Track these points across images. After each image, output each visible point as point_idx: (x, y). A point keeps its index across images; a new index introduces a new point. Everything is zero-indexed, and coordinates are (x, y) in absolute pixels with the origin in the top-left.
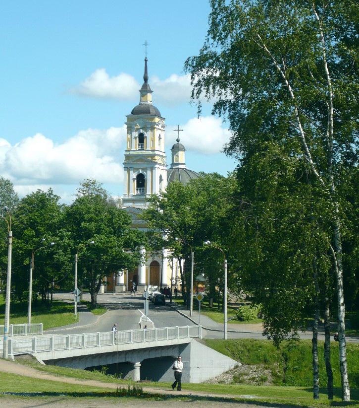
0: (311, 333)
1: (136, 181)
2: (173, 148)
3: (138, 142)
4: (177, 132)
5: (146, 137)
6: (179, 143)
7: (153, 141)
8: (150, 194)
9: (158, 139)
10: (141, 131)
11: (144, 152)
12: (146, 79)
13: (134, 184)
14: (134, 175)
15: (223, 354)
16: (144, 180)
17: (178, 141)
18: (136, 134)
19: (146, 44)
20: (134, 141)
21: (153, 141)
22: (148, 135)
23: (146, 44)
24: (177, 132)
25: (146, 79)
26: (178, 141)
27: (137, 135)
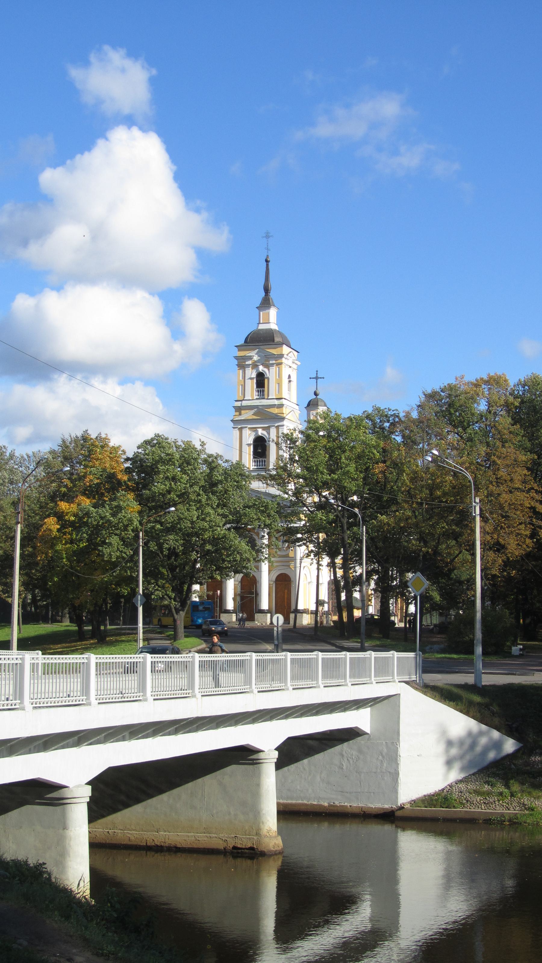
0: (402, 946)
1: (252, 446)
2: (309, 405)
3: (252, 457)
4: (315, 380)
5: (268, 379)
6: (318, 397)
7: (278, 384)
8: (269, 615)
9: (287, 380)
10: (261, 368)
11: (265, 402)
12: (267, 290)
13: (251, 386)
14: (249, 437)
15: (399, 714)
16: (266, 446)
17: (316, 394)
18: (251, 373)
19: (267, 236)
20: (249, 383)
21: (279, 384)
22: (271, 374)
23: (267, 236)
24: (314, 376)
25: (267, 290)
26: (316, 394)
27: (254, 375)
